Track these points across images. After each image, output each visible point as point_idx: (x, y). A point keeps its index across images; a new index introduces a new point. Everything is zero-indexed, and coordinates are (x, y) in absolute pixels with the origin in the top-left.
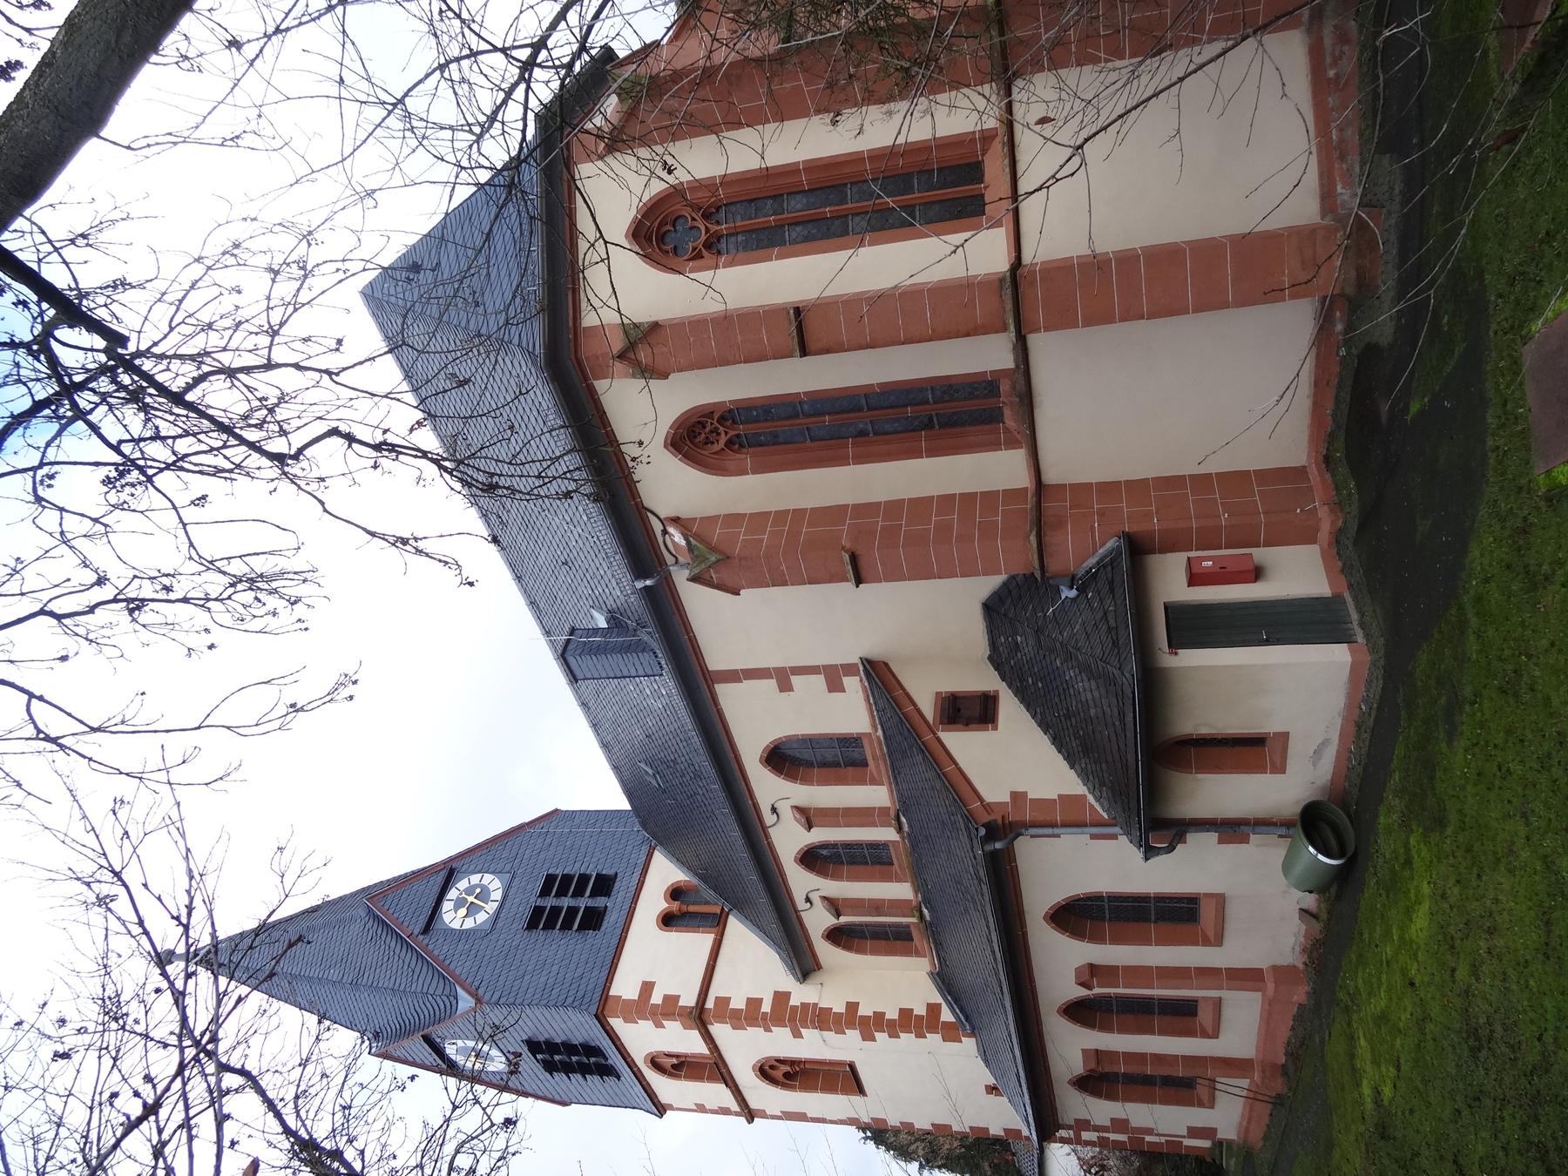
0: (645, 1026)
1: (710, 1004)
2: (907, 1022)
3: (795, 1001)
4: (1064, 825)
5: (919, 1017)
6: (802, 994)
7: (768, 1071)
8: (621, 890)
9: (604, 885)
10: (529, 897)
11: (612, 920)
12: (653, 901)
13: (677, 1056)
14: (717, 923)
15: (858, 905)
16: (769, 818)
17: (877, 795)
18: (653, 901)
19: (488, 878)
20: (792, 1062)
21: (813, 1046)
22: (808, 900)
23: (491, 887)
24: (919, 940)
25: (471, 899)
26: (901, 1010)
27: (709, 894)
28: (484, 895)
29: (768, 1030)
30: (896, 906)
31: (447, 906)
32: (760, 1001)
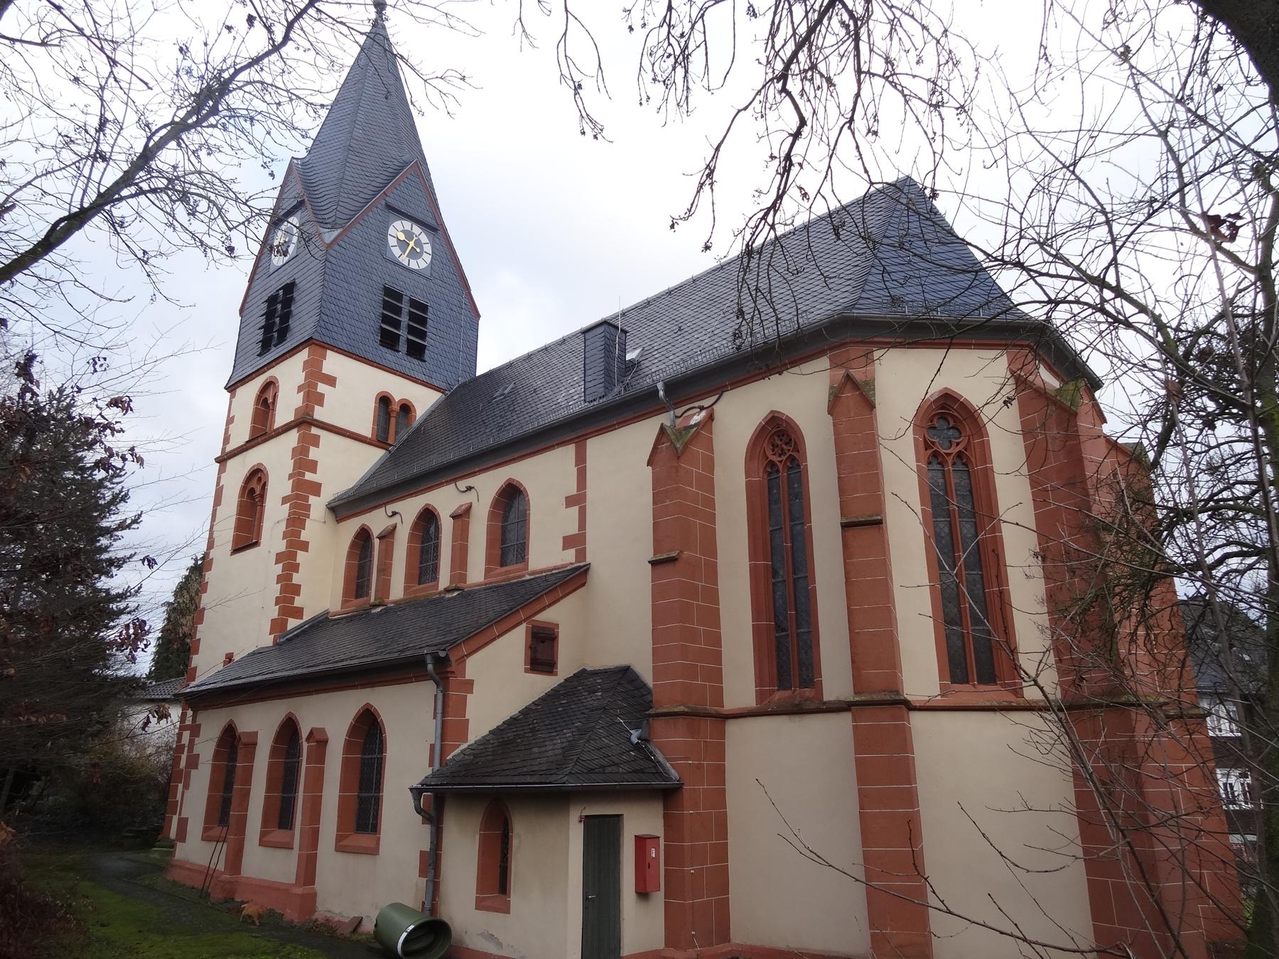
1: (314, 431)
2: (289, 590)
4: (443, 723)
6: (317, 505)
8: (411, 364)
9: (416, 351)
10: (411, 290)
11: (388, 356)
12: (401, 389)
13: (274, 403)
14: (379, 440)
15: (387, 554)
16: (462, 484)
17: (476, 573)
18: (401, 389)
19: (428, 258)
20: (262, 496)
21: (275, 512)
22: (394, 514)
23: (420, 261)
25: (412, 244)
27: (404, 435)
28: (414, 254)
29: (291, 476)
30: (385, 585)
31: (407, 225)
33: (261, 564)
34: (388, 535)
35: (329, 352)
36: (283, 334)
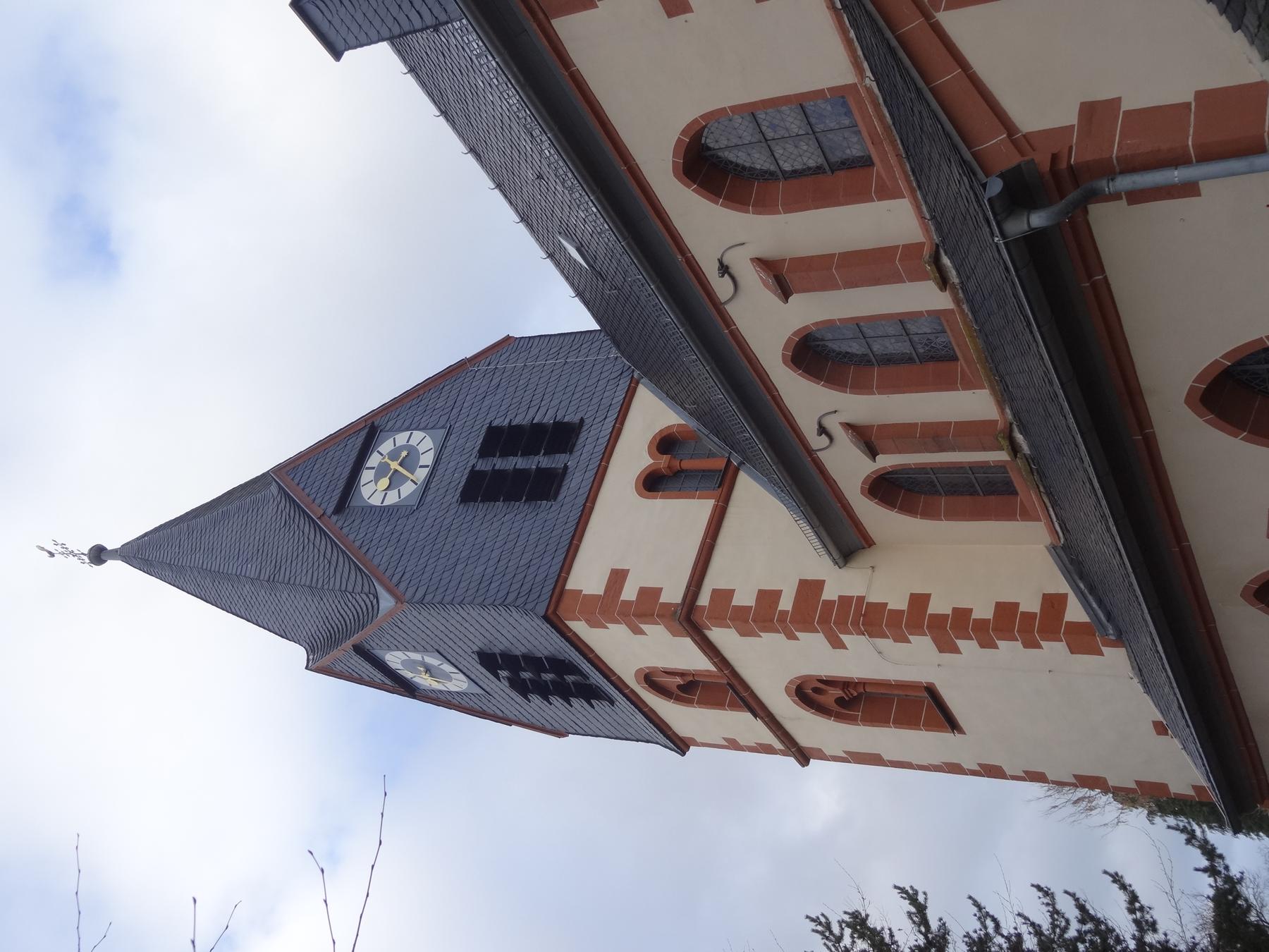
0: (772, 641)
1: (704, 600)
2: (1007, 623)
3: (830, 593)
4: (1207, 155)
5: (1029, 617)
6: (841, 583)
7: (809, 693)
8: (588, 445)
9: (562, 436)
10: (466, 457)
11: (575, 484)
12: (633, 455)
13: (682, 674)
14: (721, 485)
15: (903, 436)
16: (722, 287)
17: (893, 220)
18: (633, 455)
19: (418, 435)
20: (845, 684)
21: (862, 659)
22: (822, 430)
23: (421, 448)
24: (1028, 494)
25: (394, 465)
26: (999, 606)
27: (711, 442)
28: (410, 461)
29: (791, 636)
30: (970, 434)
31: (367, 476)
32: (776, 595)
33: (960, 674)
34: (868, 439)
35: (570, 585)
36: (561, 666)
